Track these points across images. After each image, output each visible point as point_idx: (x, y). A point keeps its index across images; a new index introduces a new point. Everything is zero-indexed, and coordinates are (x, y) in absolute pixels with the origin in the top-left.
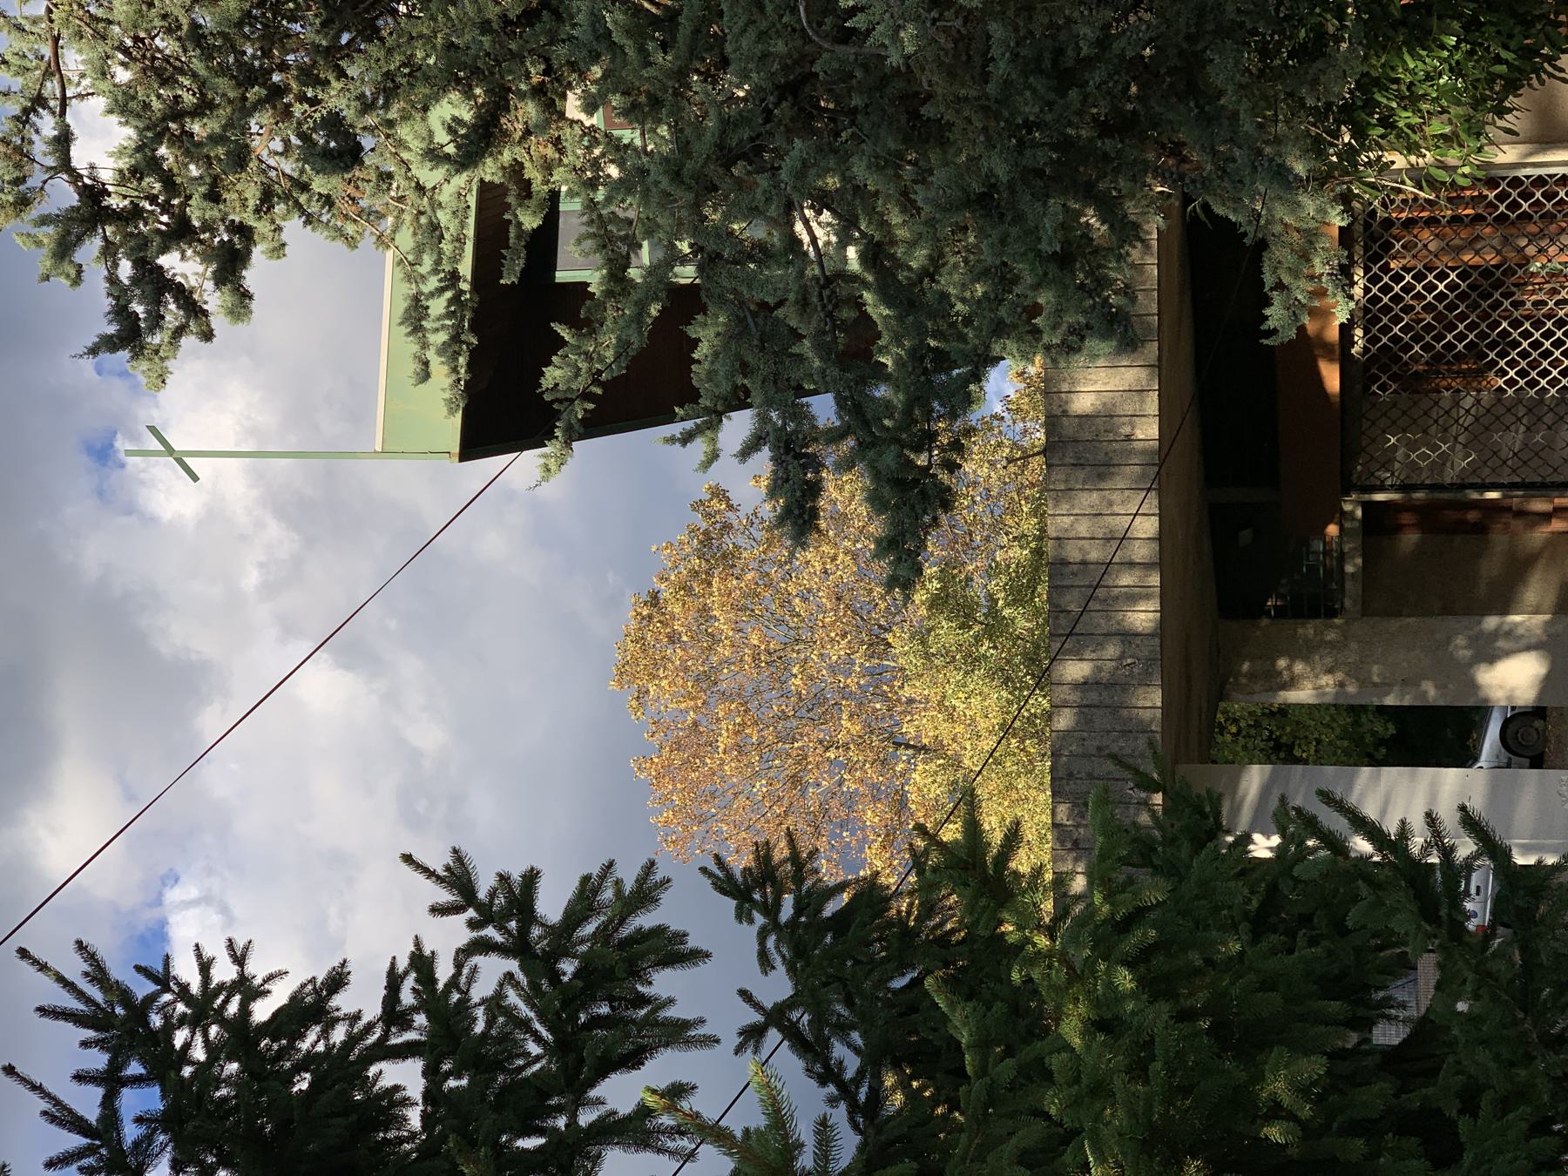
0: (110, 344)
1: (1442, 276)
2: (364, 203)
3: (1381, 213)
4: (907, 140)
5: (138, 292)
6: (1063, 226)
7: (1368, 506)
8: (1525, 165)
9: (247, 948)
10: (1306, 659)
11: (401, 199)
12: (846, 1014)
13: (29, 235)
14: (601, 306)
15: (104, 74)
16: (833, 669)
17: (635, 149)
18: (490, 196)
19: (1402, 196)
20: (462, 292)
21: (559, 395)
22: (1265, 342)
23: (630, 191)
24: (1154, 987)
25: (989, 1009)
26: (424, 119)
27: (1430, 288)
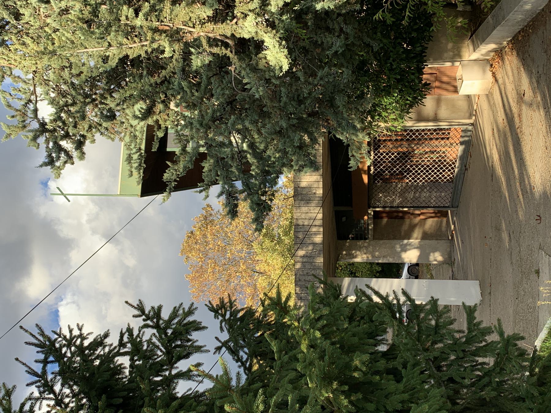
0: (46, 164)
1: (393, 154)
2: (116, 129)
3: (378, 138)
4: (260, 117)
5: (54, 150)
6: (300, 139)
7: (374, 212)
8: (413, 126)
9: (82, 326)
10: (359, 251)
11: (126, 129)
12: (243, 343)
13: (25, 135)
14: (179, 157)
15: (47, 94)
17: (188, 117)
18: (150, 129)
19: (383, 134)
20: (142, 153)
21: (168, 180)
22: (349, 170)
23: (187, 128)
24: (326, 336)
25: (281, 342)
26: (133, 108)
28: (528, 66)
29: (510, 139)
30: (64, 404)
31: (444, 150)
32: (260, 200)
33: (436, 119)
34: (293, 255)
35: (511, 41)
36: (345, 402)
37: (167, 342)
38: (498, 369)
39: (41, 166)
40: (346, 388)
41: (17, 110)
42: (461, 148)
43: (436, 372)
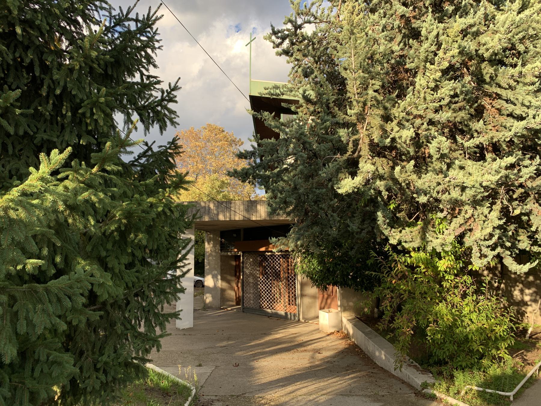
0: (273, 29)
1: (279, 267)
7: (240, 256)
16: (211, 163)
18: (297, 102)
23: (298, 126)
24: (159, 214)
27: (277, 265)
28: (338, 355)
29: (290, 345)
30: (107, 33)
31: (282, 301)
32: (250, 175)
33: (302, 295)
34: (209, 201)
35: (355, 344)
36: (113, 228)
37: (152, 107)
38: (136, 334)
39: (272, 26)
40: (123, 229)
41: (310, 10)
42: (283, 313)
43: (134, 292)
